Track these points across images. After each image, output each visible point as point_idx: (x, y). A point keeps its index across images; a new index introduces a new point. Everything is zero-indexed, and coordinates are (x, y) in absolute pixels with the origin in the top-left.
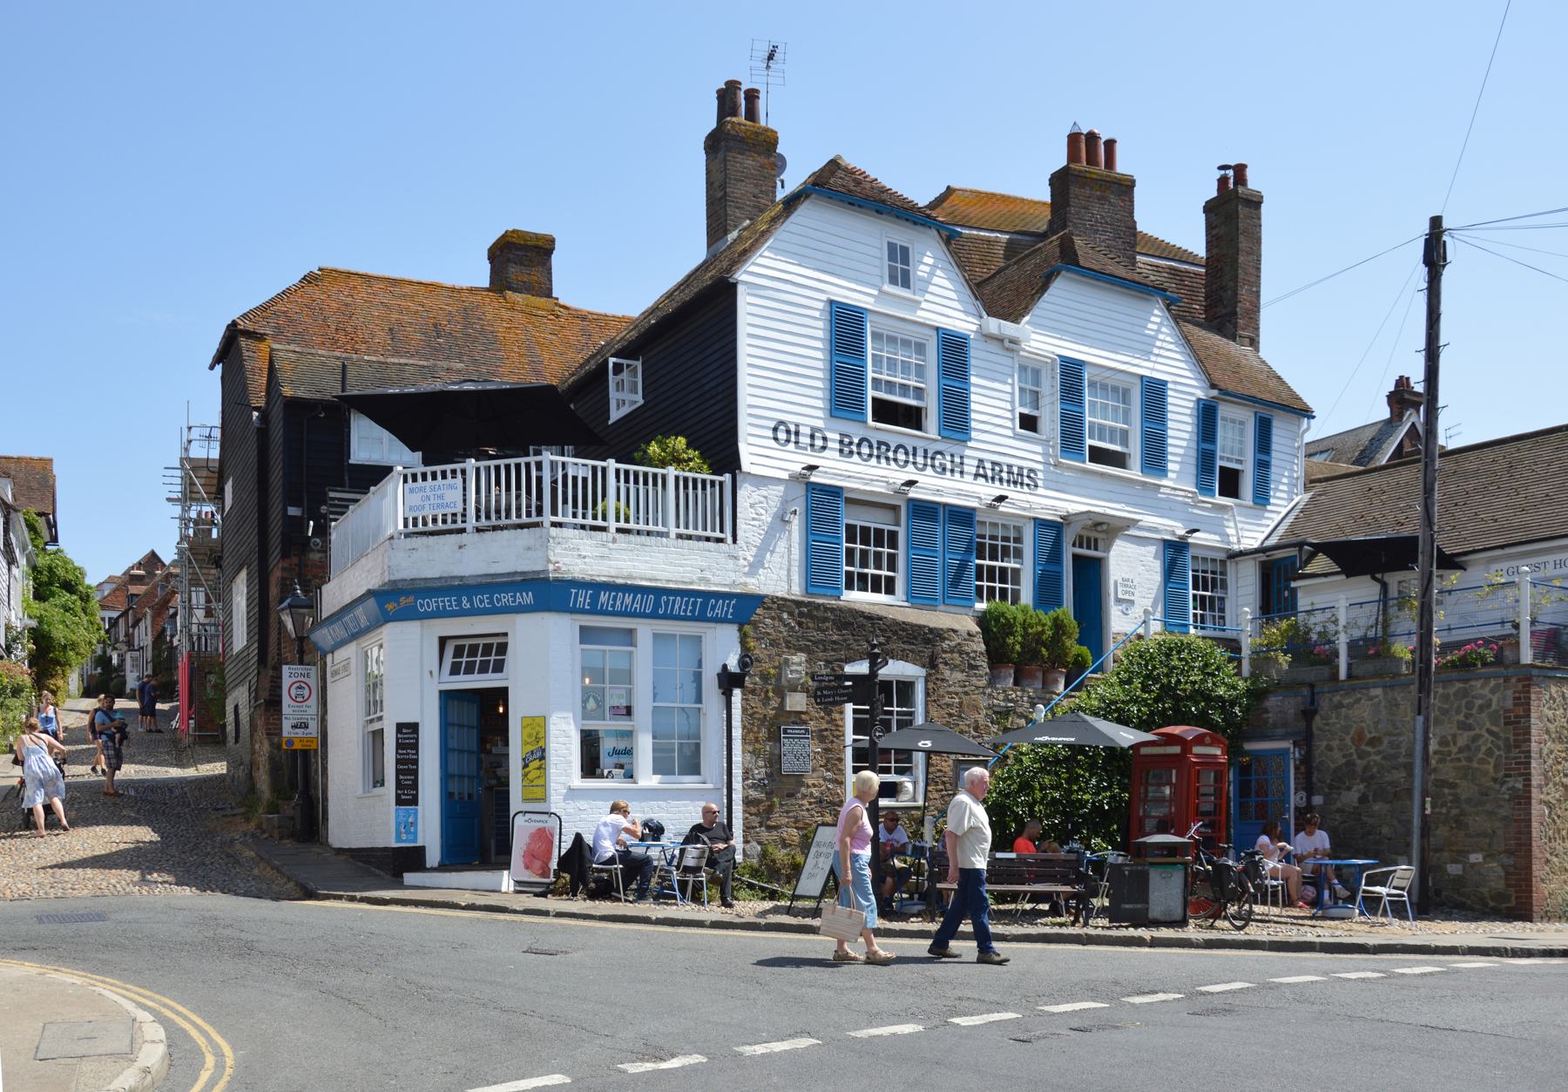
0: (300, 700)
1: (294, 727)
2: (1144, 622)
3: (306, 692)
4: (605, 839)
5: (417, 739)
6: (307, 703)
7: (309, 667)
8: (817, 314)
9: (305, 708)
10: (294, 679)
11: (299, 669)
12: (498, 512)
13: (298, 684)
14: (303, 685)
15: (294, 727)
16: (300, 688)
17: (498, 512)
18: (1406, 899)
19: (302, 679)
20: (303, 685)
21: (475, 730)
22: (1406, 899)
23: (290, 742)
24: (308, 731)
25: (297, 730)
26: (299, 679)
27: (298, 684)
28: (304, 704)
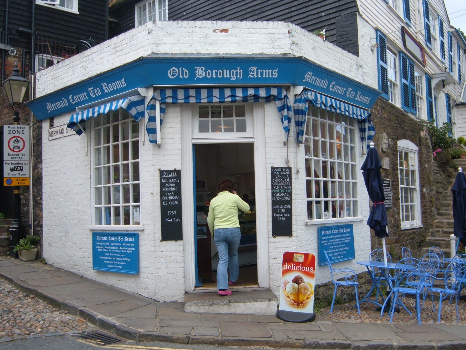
0: (17, 150)
1: (13, 170)
2: (184, 277)
3: (21, 145)
4: (97, 315)
5: (180, 201)
6: (22, 152)
7: (23, 126)
8: (385, 182)
9: (20, 156)
10: (12, 135)
11: (16, 127)
12: (348, 205)
13: (15, 139)
14: (19, 139)
15: (13, 170)
16: (17, 141)
17: (348, 205)
18: (30, 100)
19: (18, 135)
20: (19, 139)
21: (4, 160)
22: (30, 100)
23: (10, 180)
24: (22, 172)
25: (14, 172)
26: (16, 135)
27: (15, 139)
28: (20, 153)
